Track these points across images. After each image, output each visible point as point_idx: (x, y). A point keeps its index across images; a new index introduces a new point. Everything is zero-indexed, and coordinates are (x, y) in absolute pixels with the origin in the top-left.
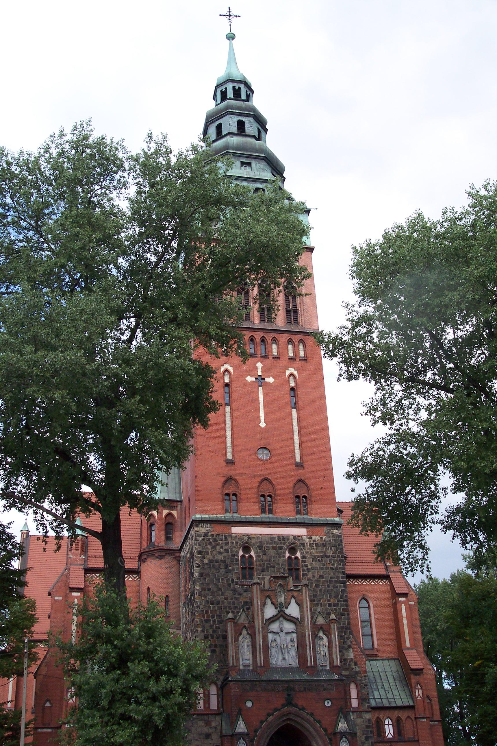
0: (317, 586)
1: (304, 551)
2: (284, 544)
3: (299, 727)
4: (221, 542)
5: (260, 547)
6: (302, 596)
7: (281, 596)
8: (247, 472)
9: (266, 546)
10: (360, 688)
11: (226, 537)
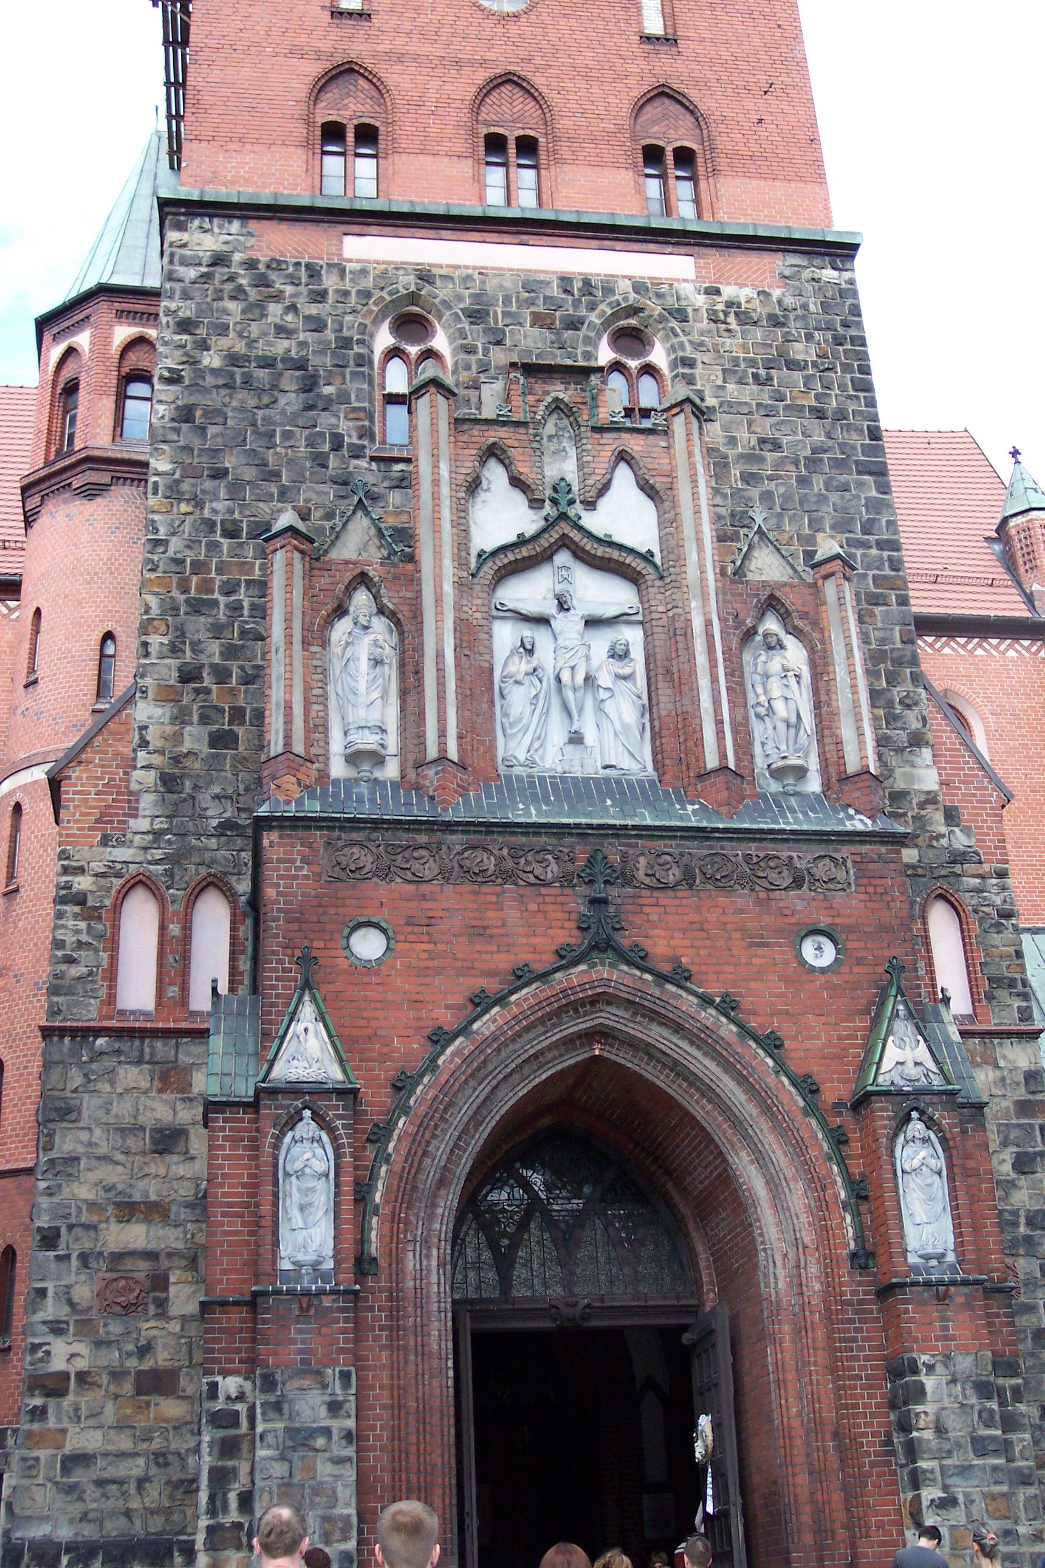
0: (749, 478)
1: (683, 338)
2: (592, 307)
3: (662, 1080)
4: (289, 289)
5: (476, 316)
6: (671, 458)
7: (561, 452)
8: (427, 49)
9: (505, 314)
10: (976, 929)
11: (314, 272)
